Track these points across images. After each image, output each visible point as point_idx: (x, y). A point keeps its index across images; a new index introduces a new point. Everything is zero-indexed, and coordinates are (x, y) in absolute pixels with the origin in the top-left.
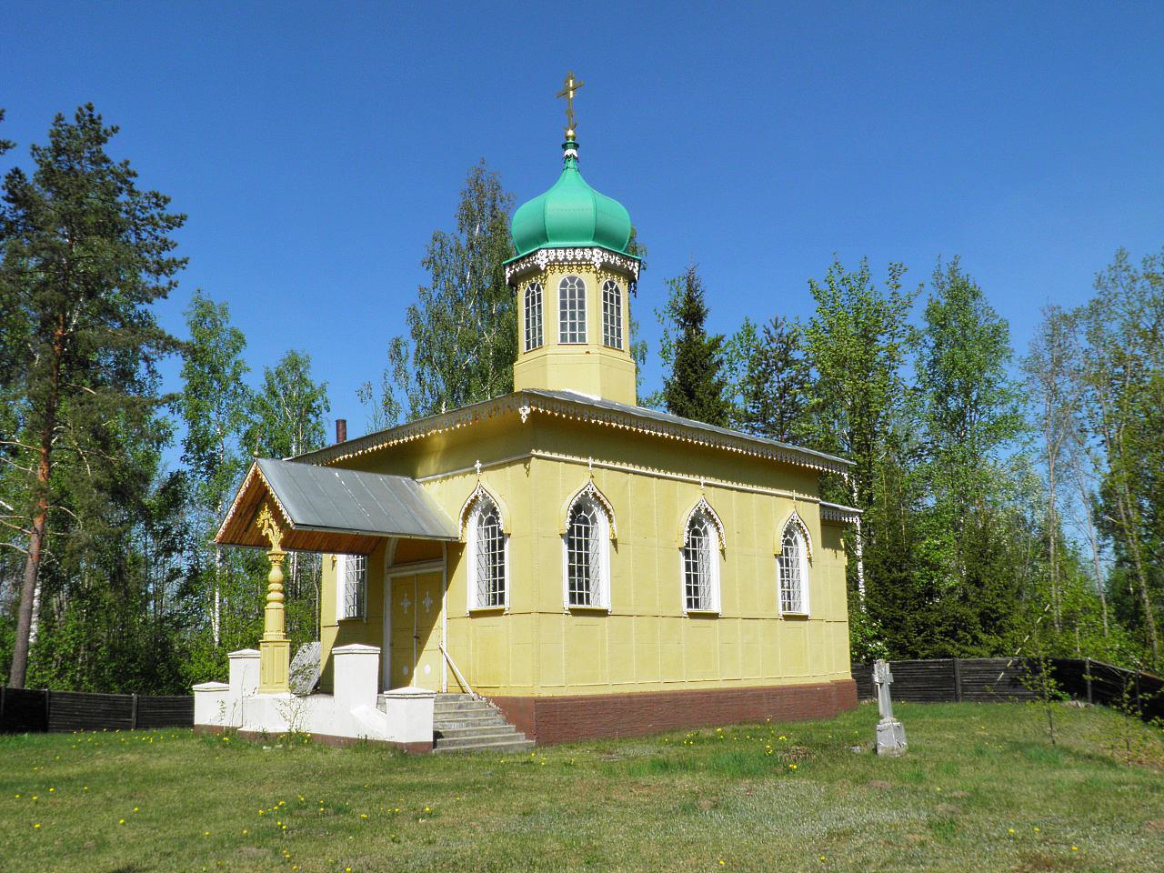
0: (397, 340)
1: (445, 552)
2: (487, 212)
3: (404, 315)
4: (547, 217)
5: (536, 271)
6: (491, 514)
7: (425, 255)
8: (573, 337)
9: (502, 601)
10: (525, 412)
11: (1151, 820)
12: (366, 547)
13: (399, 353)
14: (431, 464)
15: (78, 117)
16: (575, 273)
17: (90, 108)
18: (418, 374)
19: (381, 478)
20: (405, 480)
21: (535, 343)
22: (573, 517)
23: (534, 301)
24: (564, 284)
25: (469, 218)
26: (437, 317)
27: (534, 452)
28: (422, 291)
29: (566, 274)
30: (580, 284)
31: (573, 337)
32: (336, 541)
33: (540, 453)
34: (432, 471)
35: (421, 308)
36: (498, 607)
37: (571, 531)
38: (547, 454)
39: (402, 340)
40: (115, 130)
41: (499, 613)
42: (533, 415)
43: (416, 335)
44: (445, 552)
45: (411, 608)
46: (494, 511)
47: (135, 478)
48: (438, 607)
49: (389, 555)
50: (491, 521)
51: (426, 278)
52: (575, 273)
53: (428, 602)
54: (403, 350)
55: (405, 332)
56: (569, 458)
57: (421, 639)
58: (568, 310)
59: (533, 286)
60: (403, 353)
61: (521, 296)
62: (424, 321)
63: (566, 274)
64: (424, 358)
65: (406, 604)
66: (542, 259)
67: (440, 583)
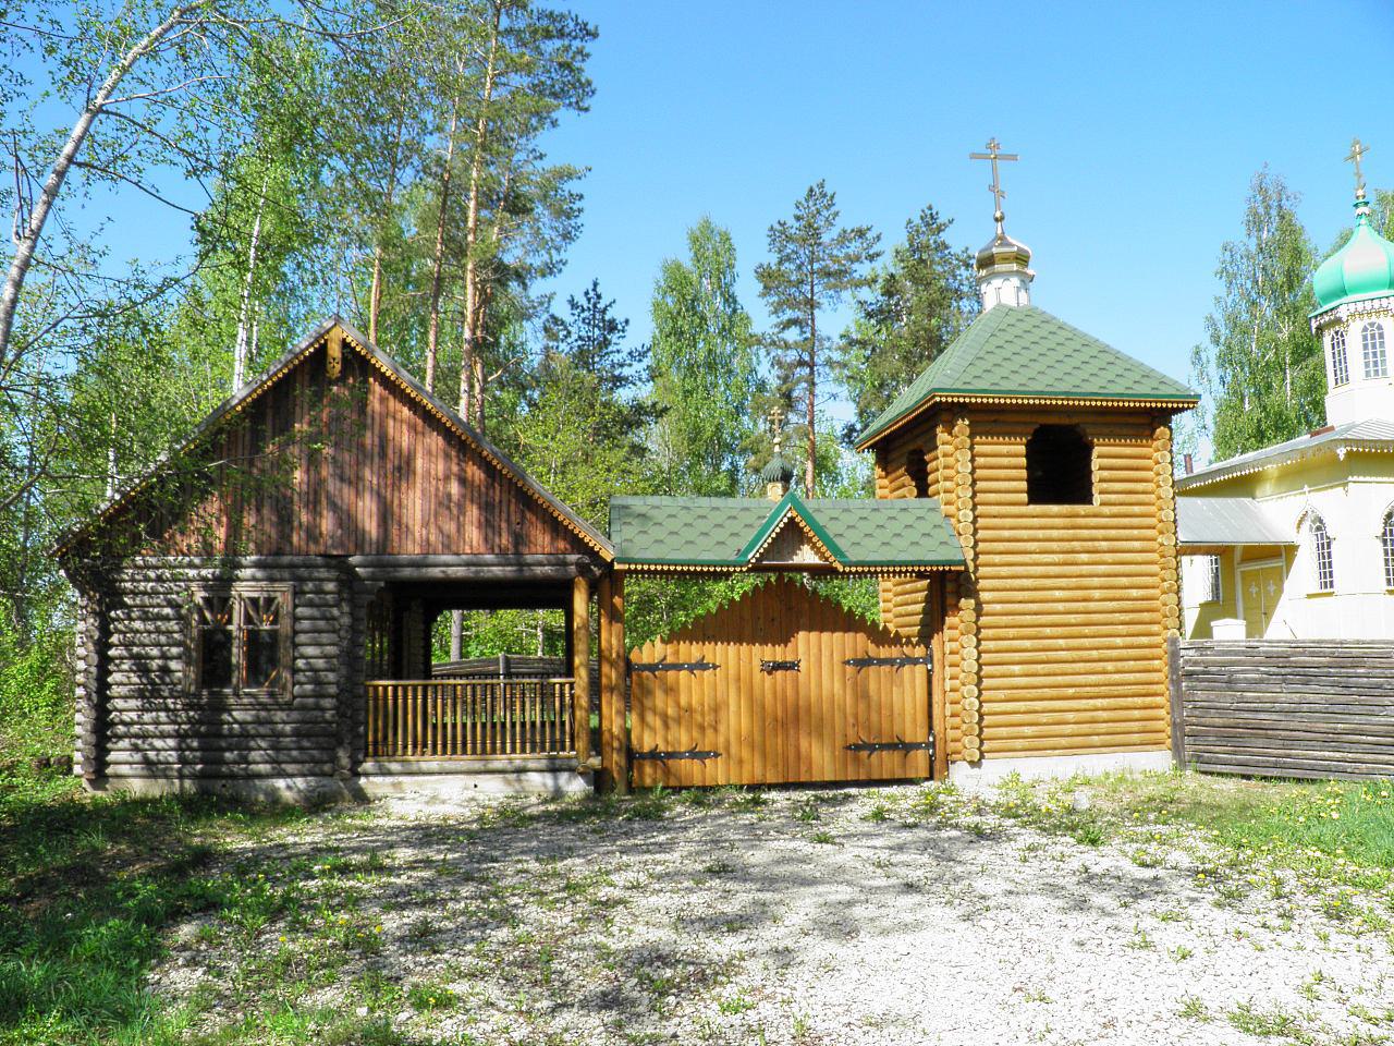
0: (1197, 347)
1: (1281, 554)
2: (1274, 212)
3: (1202, 323)
4: (1345, 278)
5: (1338, 321)
6: (1320, 525)
7: (1219, 267)
8: (1377, 372)
9: (1332, 586)
10: (1342, 452)
11: (593, 588)
12: (1222, 554)
13: (1200, 359)
14: (1267, 488)
15: (922, 218)
16: (1374, 319)
17: (930, 208)
18: (1221, 377)
19: (1231, 501)
20: (1247, 500)
21: (1342, 379)
22: (1386, 523)
23: (1339, 342)
24: (1365, 329)
25: (1256, 222)
26: (1233, 322)
27: (1350, 478)
28: (1218, 300)
29: (1366, 320)
30: (1380, 327)
31: (1377, 372)
32: (1193, 549)
33: (1355, 478)
34: (1269, 492)
35: (1218, 316)
36: (1329, 590)
37: (1385, 534)
38: (1361, 479)
39: (1202, 347)
40: (951, 222)
41: (1331, 594)
42: (1349, 454)
43: (1216, 341)
44: (1281, 554)
45: (1258, 593)
46: (1321, 521)
47: (339, 144)
48: (1280, 590)
49: (1238, 556)
50: (1318, 529)
51: (1220, 287)
52: (1374, 319)
53: (1272, 588)
54: (1203, 355)
55: (1205, 339)
56: (1380, 479)
57: (1268, 614)
58: (1369, 342)
59: (1337, 333)
60: (1204, 360)
61: (1327, 340)
62: (1224, 332)
63: (1366, 320)
64: (1225, 360)
65: (1254, 590)
66: (1343, 313)
67: (1280, 576)
